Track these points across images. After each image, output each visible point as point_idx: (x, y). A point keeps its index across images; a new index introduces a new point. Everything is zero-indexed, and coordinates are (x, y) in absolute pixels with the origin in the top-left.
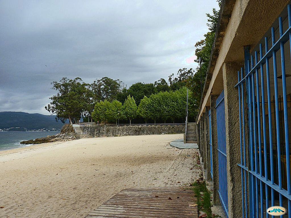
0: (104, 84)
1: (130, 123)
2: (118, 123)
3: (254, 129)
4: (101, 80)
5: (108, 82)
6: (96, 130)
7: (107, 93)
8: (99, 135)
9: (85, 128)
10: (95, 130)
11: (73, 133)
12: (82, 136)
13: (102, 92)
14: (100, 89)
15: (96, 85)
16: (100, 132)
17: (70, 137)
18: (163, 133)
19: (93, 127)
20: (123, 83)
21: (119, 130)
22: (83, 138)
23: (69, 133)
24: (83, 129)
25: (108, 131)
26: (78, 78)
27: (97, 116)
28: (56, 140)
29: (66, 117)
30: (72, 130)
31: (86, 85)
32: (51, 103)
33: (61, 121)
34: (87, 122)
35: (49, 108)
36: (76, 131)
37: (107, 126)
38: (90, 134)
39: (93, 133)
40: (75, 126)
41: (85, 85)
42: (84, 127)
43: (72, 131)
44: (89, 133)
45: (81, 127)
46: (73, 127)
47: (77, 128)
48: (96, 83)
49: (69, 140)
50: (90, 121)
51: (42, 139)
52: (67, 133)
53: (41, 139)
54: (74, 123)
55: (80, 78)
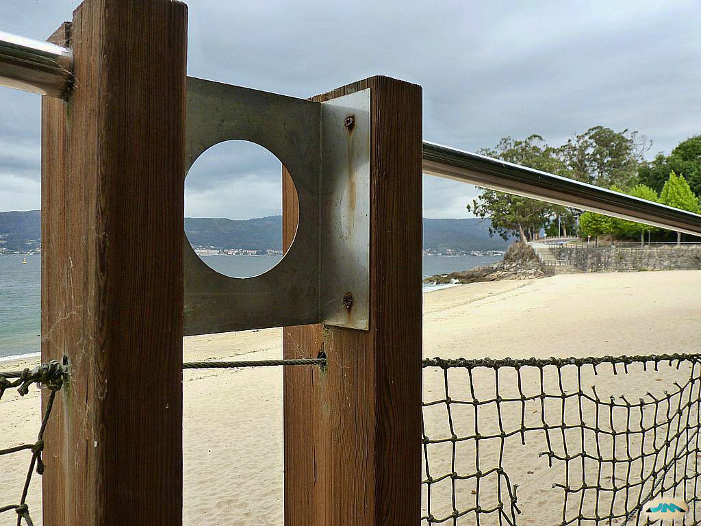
0: (595, 144)
1: (642, 240)
2: (646, 240)
3: (66, 428)
4: (586, 134)
5: (603, 138)
6: (590, 256)
7: (601, 166)
8: (599, 266)
9: (562, 250)
10: (587, 256)
11: (535, 263)
12: (558, 268)
13: (587, 163)
14: (583, 155)
15: (574, 149)
16: (600, 260)
17: (530, 271)
18: (102, 307)
19: (583, 249)
20: (643, 136)
21: (650, 256)
22: (562, 272)
23: (520, 262)
24: (559, 253)
25: (621, 257)
26: (535, 136)
27: (594, 224)
28: (500, 277)
29: (513, 225)
30: (533, 255)
31: (554, 151)
32: (479, 197)
33: (500, 235)
34: (555, 235)
35: (476, 208)
36: (543, 258)
37: (617, 247)
38: (576, 265)
39: (581, 264)
40: (536, 246)
41: (548, 150)
42: (560, 248)
43: (531, 258)
44: (573, 262)
45: (551, 249)
46: (533, 250)
47: (542, 250)
48: (574, 143)
49: (530, 277)
50: (562, 234)
51: (467, 273)
52: (520, 262)
53: (465, 275)
54: (528, 240)
55: (538, 137)
